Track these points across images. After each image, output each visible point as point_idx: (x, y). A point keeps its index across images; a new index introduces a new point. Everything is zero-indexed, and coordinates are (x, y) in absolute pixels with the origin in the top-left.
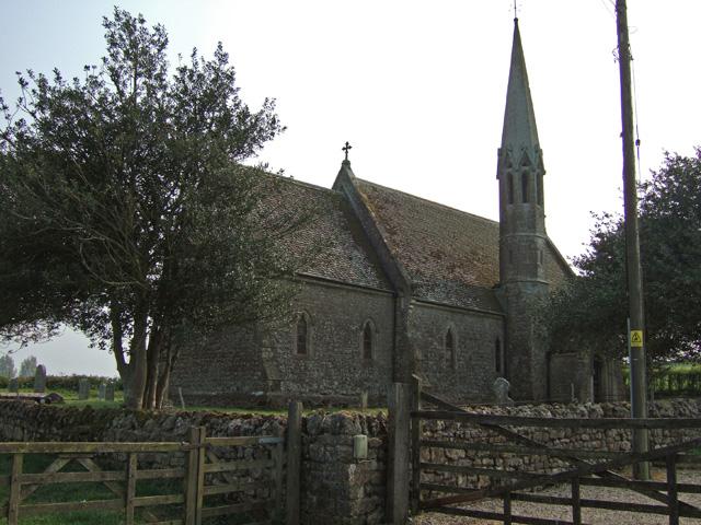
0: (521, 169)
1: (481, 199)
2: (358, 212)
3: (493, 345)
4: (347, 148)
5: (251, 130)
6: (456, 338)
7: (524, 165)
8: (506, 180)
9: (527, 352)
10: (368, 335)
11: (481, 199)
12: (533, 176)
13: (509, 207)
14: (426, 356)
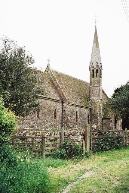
0: (96, 72)
1: (85, 77)
2: (52, 79)
3: (88, 116)
4: (49, 60)
5: (30, 60)
6: (78, 114)
7: (97, 67)
8: (92, 71)
9: (97, 118)
10: (55, 113)
11: (85, 77)
12: (99, 70)
13: (93, 78)
14: (71, 119)
